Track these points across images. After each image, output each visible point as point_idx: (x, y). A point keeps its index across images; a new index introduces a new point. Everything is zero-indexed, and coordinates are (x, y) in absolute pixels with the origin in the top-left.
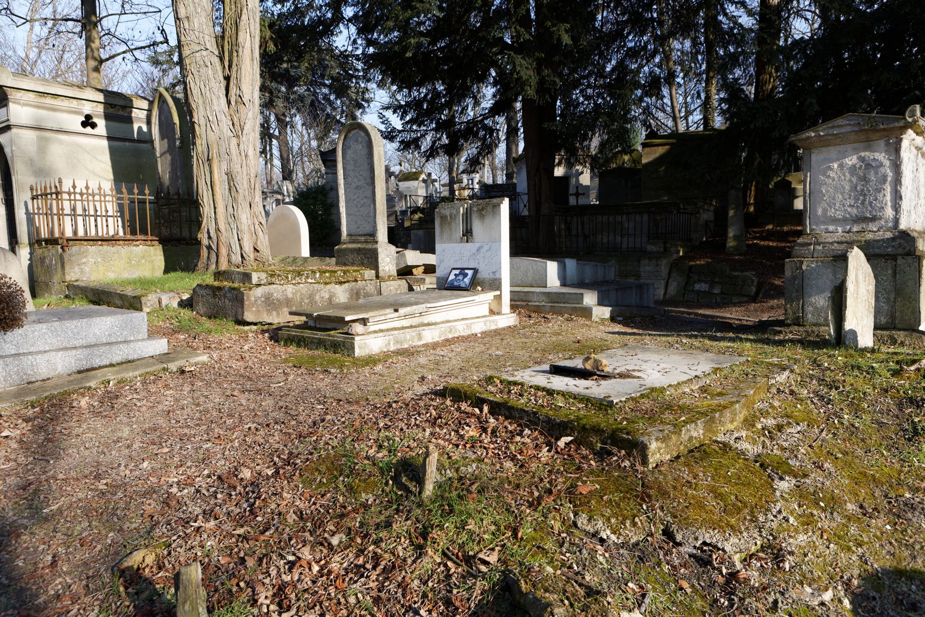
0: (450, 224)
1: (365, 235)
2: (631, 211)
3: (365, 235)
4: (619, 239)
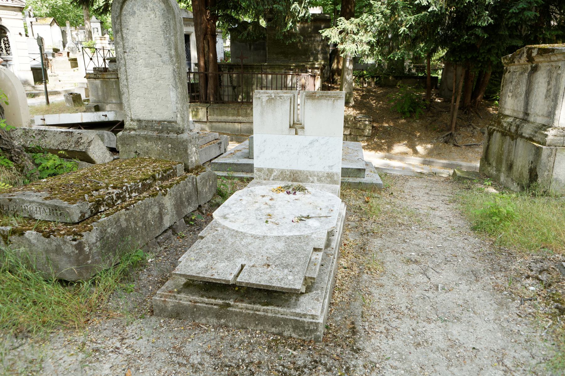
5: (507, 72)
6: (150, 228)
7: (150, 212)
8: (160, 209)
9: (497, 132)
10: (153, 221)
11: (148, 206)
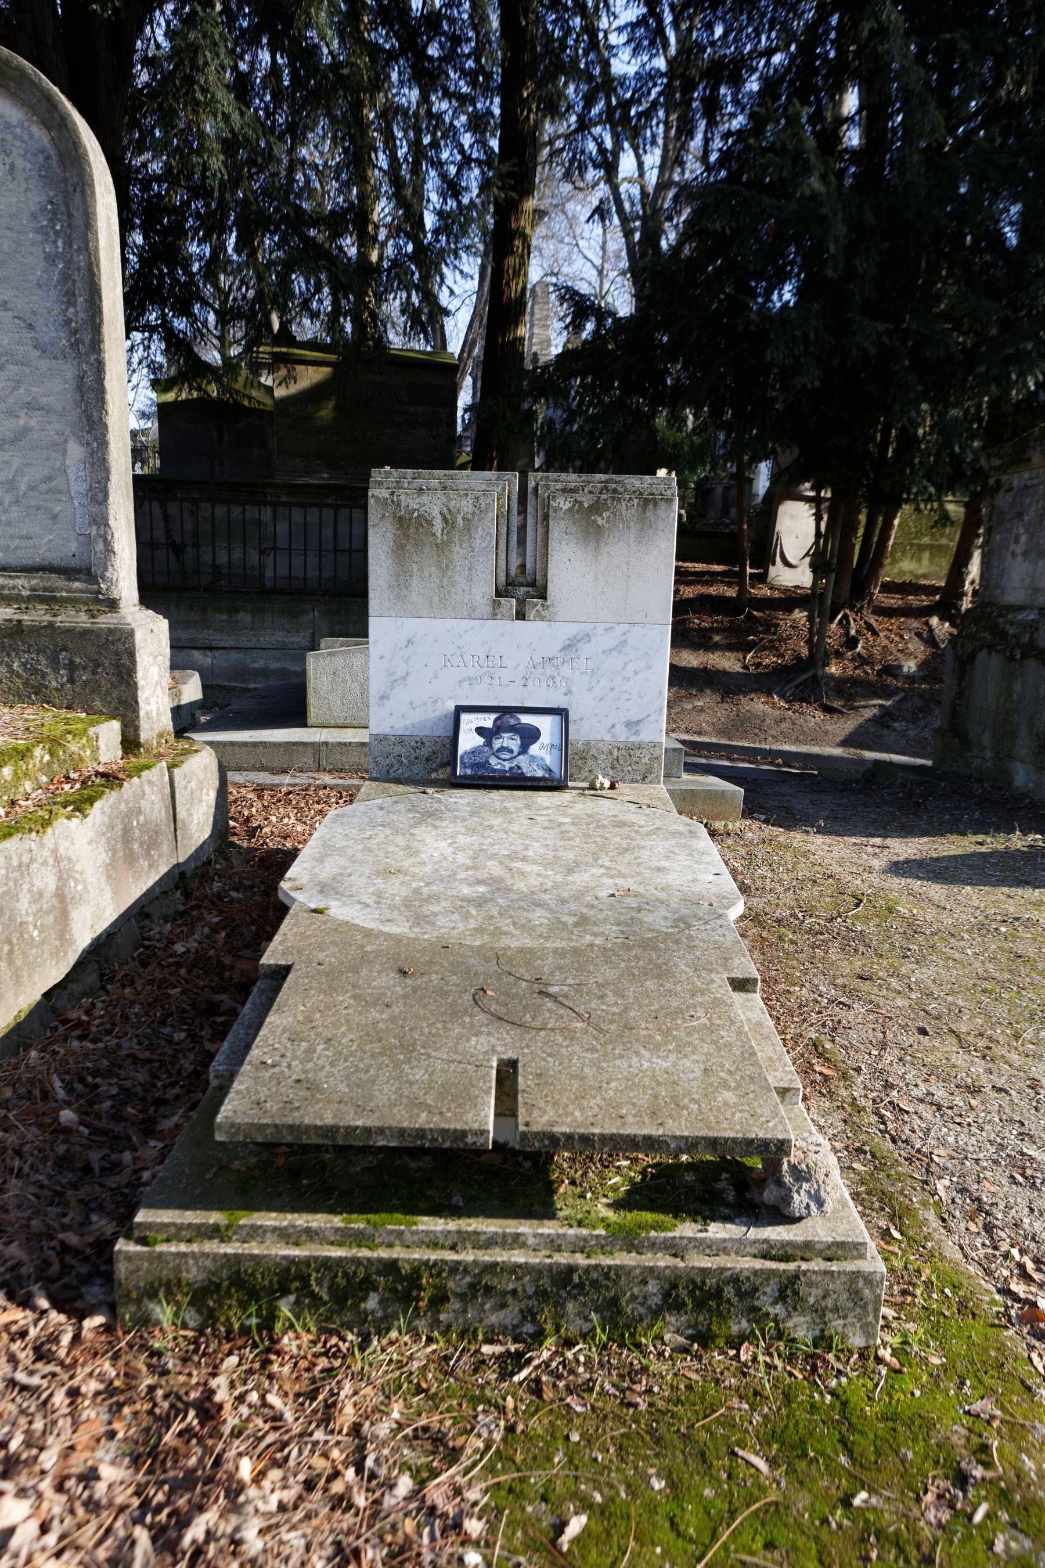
0: (442, 548)
1: (28, 570)
2: (284, 499)
3: (28, 570)
4: (254, 557)
5: (1002, 492)
6: (25, 955)
7: (25, 887)
8: (60, 878)
9: (990, 653)
10: (35, 927)
11: (20, 865)
